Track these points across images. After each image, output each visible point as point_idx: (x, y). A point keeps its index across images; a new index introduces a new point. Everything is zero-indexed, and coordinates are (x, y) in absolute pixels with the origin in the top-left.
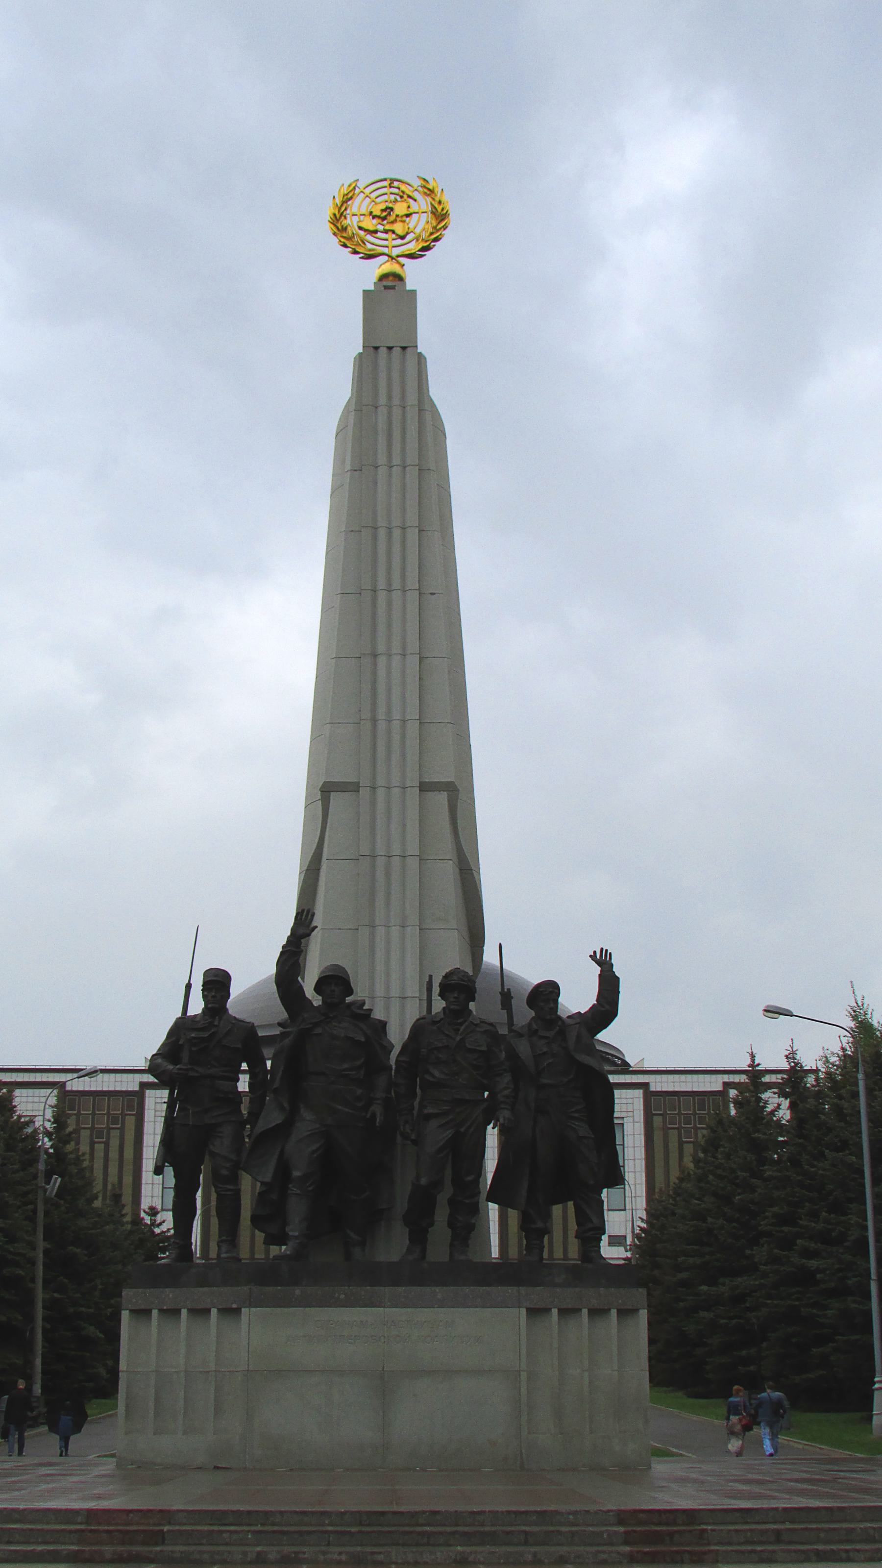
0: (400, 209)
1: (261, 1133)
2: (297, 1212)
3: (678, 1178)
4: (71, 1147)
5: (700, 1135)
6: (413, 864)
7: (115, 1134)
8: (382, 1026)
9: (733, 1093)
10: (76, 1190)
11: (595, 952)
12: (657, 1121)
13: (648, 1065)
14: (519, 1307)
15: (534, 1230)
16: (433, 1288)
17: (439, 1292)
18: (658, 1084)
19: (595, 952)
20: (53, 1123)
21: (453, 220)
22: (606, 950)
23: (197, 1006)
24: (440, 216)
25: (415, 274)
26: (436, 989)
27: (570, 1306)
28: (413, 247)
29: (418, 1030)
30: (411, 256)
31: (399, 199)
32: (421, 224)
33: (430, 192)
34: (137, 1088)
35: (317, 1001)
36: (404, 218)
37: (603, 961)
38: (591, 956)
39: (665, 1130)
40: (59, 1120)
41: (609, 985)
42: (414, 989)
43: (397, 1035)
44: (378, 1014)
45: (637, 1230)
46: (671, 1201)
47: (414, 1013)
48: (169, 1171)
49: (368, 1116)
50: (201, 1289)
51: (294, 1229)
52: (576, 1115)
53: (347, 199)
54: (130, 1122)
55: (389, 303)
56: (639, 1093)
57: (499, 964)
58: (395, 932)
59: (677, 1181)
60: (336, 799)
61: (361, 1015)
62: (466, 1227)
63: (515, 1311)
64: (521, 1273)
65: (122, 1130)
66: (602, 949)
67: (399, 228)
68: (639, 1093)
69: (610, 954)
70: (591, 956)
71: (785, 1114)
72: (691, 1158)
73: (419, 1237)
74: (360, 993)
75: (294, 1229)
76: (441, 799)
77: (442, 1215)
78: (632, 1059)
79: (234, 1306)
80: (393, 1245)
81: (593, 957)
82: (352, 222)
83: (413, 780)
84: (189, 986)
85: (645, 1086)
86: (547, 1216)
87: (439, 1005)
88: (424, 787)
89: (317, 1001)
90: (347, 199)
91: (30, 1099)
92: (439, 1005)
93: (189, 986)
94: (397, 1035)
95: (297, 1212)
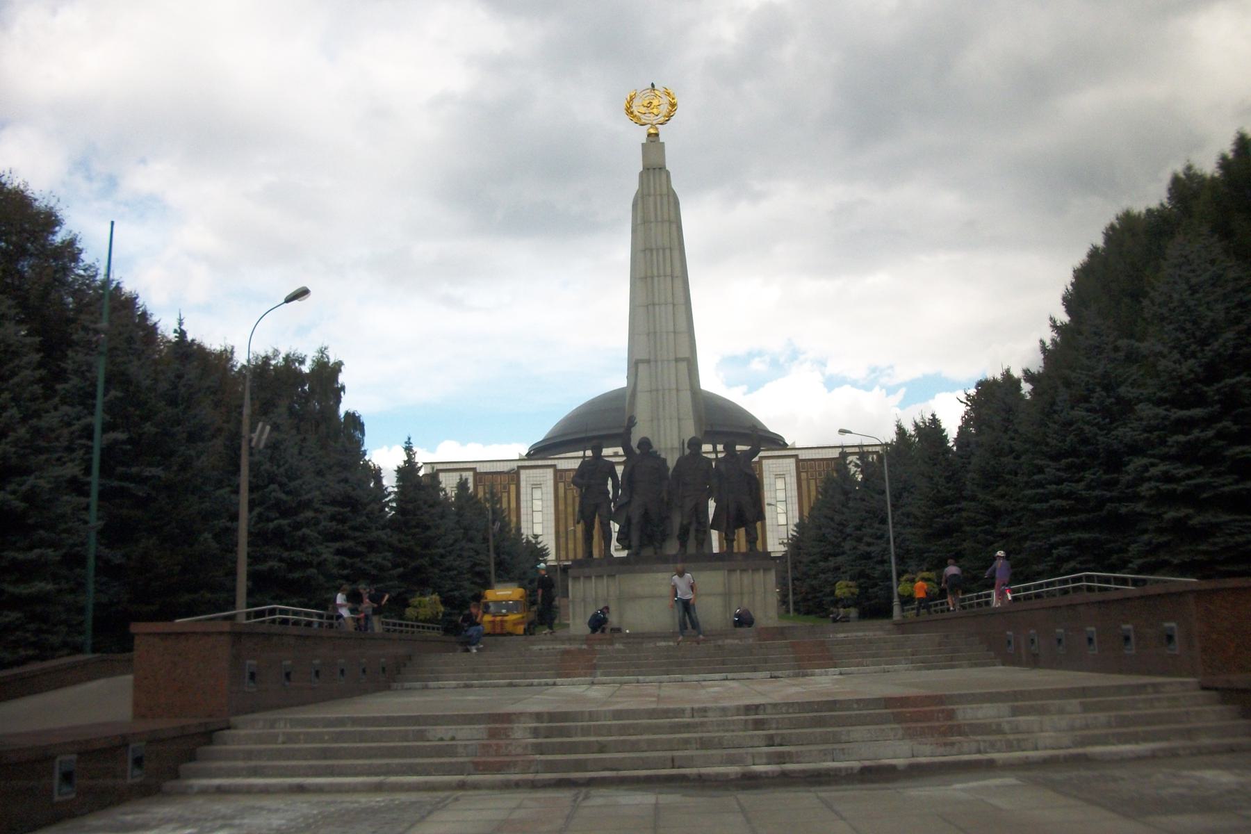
0: (655, 102)
6: (674, 392)
8: (665, 460)
12: (804, 475)
15: (728, 539)
18: (803, 455)
24: (673, 105)
28: (662, 119)
32: (665, 109)
35: (638, 451)
39: (808, 480)
42: (676, 444)
43: (671, 462)
44: (663, 456)
47: (676, 456)
53: (632, 99)
54: (513, 488)
56: (793, 461)
60: (641, 367)
61: (655, 457)
62: (704, 540)
64: (726, 556)
65: (509, 493)
67: (655, 111)
68: (793, 461)
71: (860, 477)
73: (683, 544)
74: (655, 446)
76: (683, 366)
77: (692, 534)
80: (672, 547)
82: (635, 109)
83: (672, 356)
85: (796, 456)
88: (677, 360)
89: (638, 451)
90: (632, 99)
91: (939, 607)
94: (671, 462)
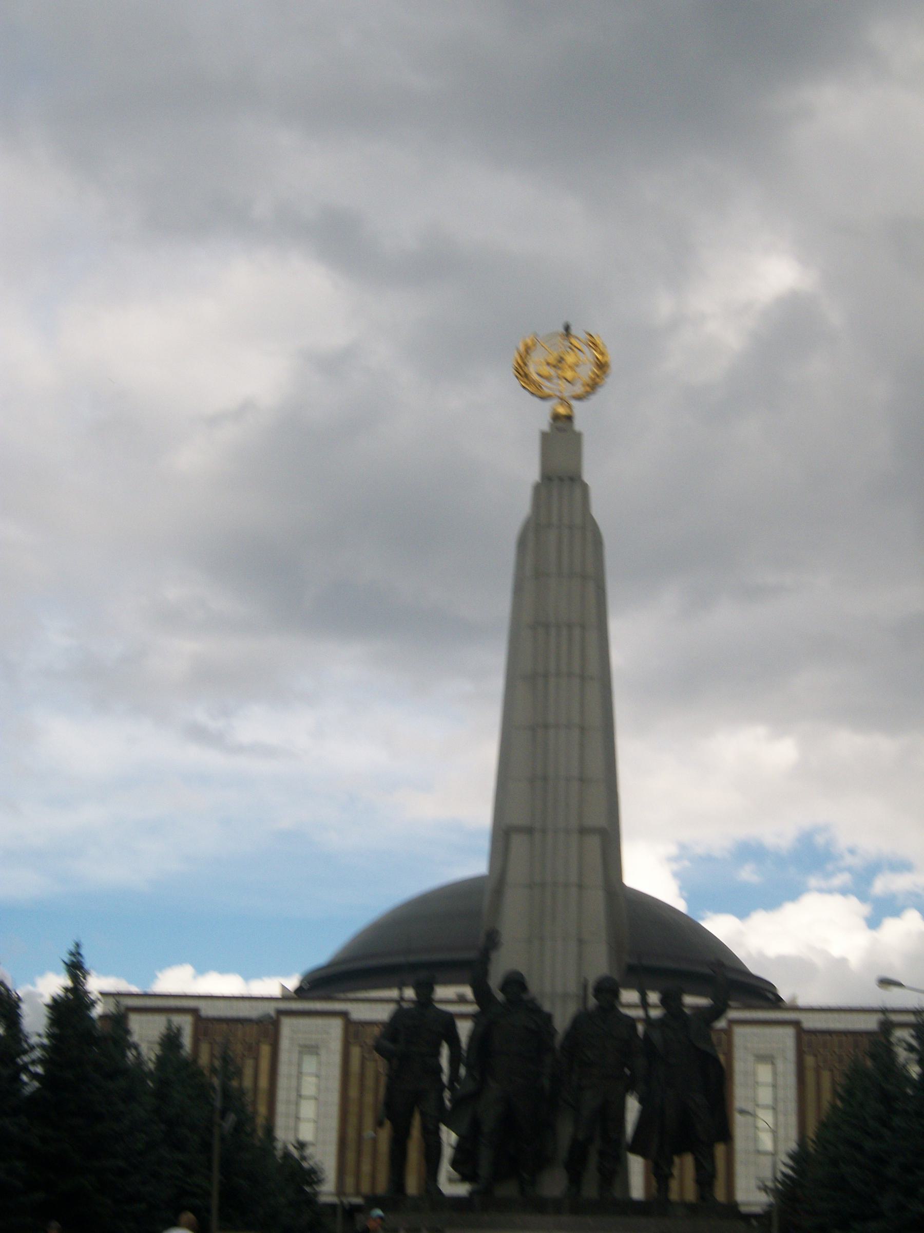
0: (570, 359)
2: (485, 1156)
4: (235, 1083)
8: (548, 1018)
10: (245, 1121)
12: (810, 1061)
13: (802, 1002)
15: (659, 1174)
18: (810, 1022)
21: (614, 368)
25: (584, 416)
26: (590, 990)
28: (579, 389)
29: (578, 1023)
30: (579, 398)
32: (587, 371)
33: (594, 345)
34: (273, 1013)
35: (500, 997)
39: (818, 1070)
43: (562, 1021)
44: (547, 1007)
48: (388, 1124)
51: (484, 1170)
54: (265, 1050)
55: (561, 438)
60: (519, 843)
61: (534, 1009)
62: (614, 1172)
65: (257, 1059)
67: (569, 374)
73: (575, 1179)
74: (534, 988)
75: (484, 1170)
77: (593, 1160)
78: (785, 993)
80: (554, 1184)
82: (532, 370)
86: (671, 1163)
88: (583, 831)
89: (500, 997)
92: (592, 1002)
94: (562, 1021)
95: (485, 1156)
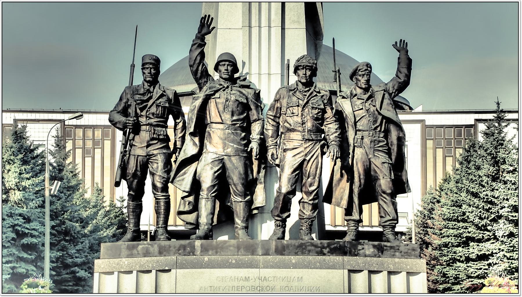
1: (182, 161)
3: (443, 180)
5: (457, 152)
7: (98, 152)
9: (482, 127)
11: (396, 43)
14: (343, 269)
16: (289, 257)
17: (294, 259)
19: (396, 43)
20: (55, 147)
22: (404, 41)
23: (139, 80)
26: (292, 69)
27: (376, 269)
31: (477, 146)
36: (303, 117)
37: (402, 48)
38: (393, 45)
40: (60, 145)
41: (406, 64)
45: (416, 211)
46: (437, 193)
49: (249, 150)
50: (146, 258)
52: (380, 149)
56: (418, 126)
57: (332, 47)
58: (265, 31)
59: (442, 182)
63: (341, 271)
66: (401, 40)
68: (418, 126)
69: (407, 43)
70: (393, 45)
72: (451, 168)
79: (167, 268)
81: (395, 46)
84: (133, 66)
87: (293, 79)
93: (133, 66)
